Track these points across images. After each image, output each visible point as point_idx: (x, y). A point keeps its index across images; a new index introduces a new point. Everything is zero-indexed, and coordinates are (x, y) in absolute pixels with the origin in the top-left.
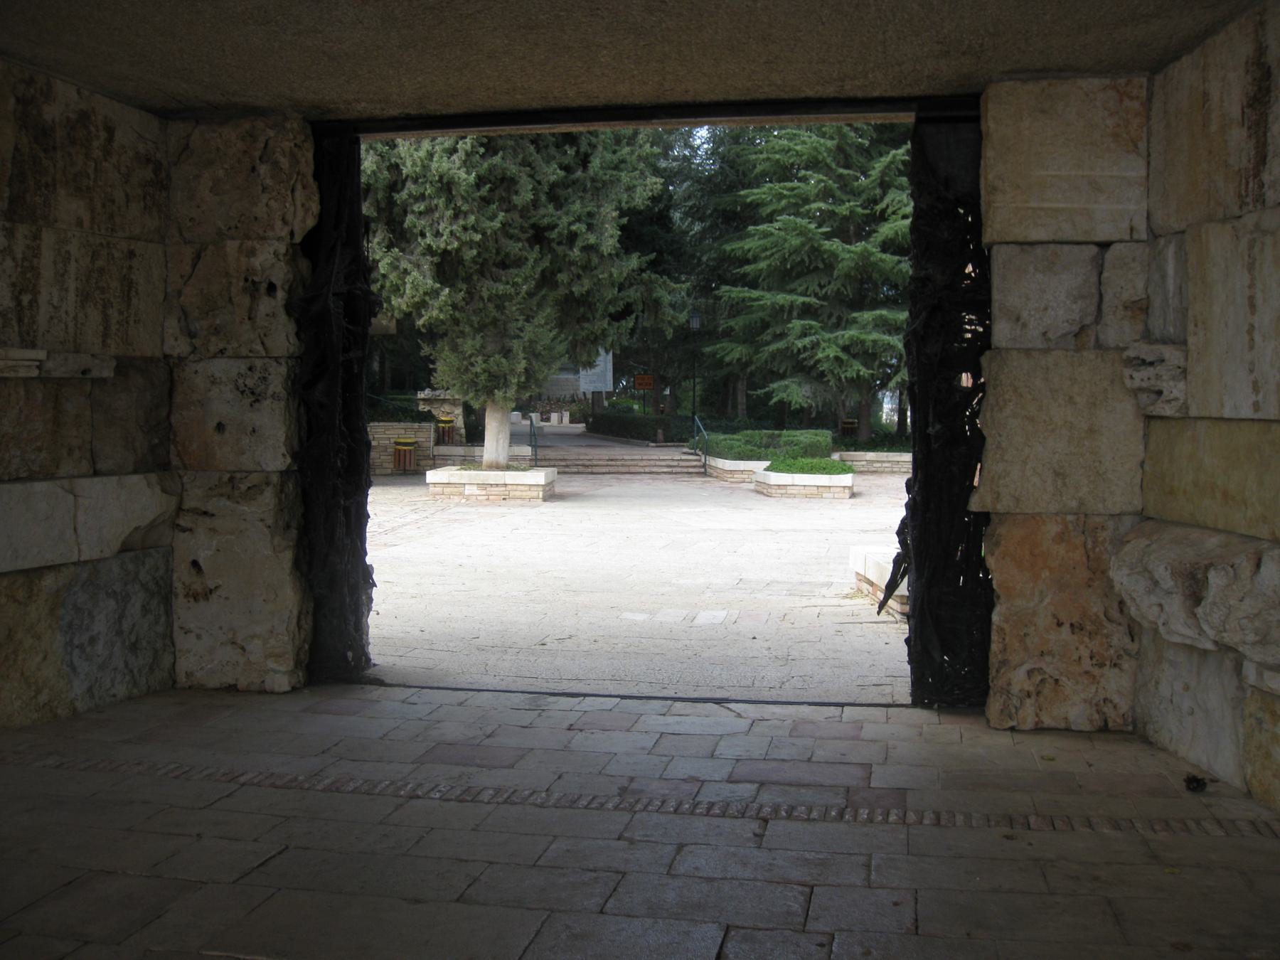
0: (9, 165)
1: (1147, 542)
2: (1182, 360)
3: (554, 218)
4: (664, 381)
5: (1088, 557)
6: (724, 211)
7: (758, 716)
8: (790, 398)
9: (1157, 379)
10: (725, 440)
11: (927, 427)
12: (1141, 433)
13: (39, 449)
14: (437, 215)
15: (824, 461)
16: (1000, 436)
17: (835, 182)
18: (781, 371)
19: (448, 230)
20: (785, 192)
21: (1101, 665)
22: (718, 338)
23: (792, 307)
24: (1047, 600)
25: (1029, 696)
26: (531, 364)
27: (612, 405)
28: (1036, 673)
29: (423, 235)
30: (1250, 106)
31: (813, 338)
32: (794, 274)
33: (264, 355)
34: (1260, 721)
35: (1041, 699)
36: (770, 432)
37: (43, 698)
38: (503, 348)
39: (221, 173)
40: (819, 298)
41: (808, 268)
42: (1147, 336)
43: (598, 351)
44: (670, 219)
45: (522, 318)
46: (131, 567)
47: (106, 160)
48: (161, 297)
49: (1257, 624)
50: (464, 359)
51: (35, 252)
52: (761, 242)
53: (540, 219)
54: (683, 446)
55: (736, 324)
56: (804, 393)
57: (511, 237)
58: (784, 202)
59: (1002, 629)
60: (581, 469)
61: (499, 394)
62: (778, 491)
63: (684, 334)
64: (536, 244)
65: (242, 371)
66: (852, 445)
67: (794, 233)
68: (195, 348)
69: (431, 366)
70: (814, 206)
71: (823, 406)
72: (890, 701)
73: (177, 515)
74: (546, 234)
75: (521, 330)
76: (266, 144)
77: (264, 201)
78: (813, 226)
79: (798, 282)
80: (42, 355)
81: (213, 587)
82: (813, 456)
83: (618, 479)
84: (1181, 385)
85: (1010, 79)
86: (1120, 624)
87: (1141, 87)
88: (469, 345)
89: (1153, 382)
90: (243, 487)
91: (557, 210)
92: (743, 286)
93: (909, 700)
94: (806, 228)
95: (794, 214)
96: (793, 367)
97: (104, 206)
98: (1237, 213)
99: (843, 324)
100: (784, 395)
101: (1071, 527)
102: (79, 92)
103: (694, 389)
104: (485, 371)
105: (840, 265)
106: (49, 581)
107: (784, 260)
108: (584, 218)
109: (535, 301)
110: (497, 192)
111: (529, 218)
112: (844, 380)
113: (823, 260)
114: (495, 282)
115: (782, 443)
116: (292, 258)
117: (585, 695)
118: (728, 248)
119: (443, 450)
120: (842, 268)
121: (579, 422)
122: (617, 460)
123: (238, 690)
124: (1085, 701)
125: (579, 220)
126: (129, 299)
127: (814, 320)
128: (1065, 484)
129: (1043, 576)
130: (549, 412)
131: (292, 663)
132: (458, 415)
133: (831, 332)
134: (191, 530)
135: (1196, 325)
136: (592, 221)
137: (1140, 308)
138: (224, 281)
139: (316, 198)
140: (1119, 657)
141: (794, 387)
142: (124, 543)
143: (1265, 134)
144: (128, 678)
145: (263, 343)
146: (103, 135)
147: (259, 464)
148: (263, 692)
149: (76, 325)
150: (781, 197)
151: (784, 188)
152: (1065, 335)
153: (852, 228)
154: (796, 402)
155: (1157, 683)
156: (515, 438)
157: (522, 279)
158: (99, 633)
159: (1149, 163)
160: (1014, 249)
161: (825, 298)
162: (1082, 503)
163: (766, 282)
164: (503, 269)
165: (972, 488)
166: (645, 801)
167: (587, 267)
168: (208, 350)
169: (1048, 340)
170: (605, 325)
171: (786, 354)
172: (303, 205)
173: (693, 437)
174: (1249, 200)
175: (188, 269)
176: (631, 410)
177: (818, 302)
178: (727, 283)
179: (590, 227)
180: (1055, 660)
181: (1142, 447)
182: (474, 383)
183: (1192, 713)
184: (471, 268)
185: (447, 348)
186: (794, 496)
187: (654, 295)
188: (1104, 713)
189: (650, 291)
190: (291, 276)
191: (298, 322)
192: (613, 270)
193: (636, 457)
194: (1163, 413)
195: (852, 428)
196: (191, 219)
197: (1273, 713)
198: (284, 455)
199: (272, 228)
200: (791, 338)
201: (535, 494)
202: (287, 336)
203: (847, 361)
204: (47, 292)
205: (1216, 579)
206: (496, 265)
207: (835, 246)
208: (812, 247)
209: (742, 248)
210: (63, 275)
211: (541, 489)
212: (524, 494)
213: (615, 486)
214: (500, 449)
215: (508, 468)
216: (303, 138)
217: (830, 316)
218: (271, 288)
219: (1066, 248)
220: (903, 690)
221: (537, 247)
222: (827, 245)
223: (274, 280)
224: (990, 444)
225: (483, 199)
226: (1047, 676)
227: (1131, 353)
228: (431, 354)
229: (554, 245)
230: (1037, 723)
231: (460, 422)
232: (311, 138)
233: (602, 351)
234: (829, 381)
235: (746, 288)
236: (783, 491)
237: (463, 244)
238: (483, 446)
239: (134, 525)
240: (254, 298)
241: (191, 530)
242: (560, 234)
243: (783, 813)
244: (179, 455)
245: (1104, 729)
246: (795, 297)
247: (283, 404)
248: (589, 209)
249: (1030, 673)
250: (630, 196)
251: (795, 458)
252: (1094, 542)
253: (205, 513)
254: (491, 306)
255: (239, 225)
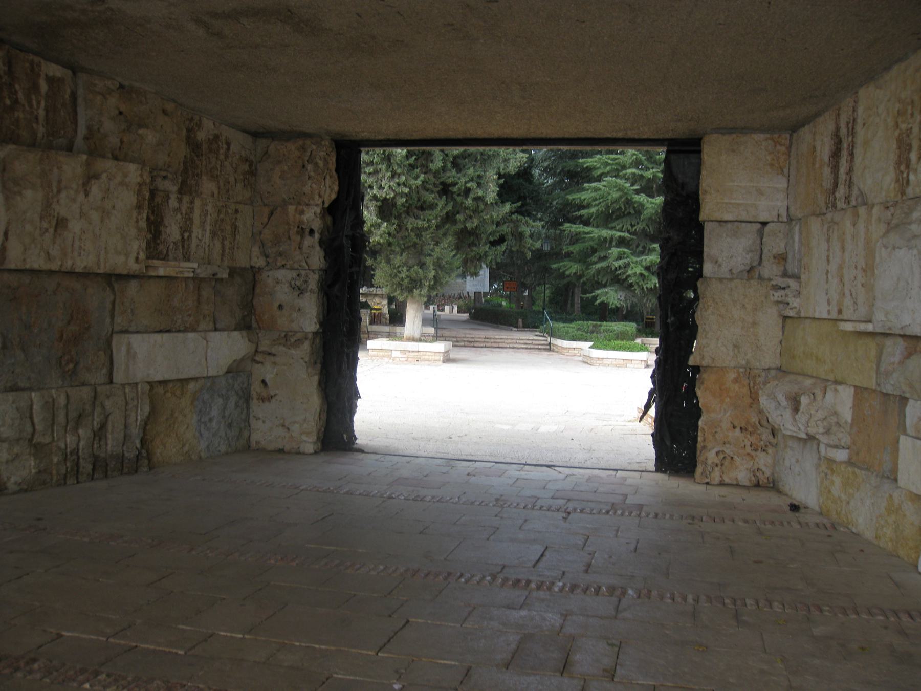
0: (182, 165)
1: (777, 383)
2: (798, 287)
3: (455, 179)
4: (524, 286)
5: (751, 391)
6: (569, 171)
7: (570, 473)
8: (608, 301)
9: (786, 296)
10: (564, 327)
11: (667, 319)
12: (781, 325)
13: (190, 315)
14: (381, 175)
15: (628, 343)
16: (705, 324)
17: (643, 155)
18: (603, 282)
19: (387, 186)
20: (609, 161)
21: (756, 450)
22: (562, 258)
23: (612, 238)
24: (728, 414)
25: (717, 466)
26: (437, 273)
27: (487, 302)
28: (721, 453)
29: (371, 187)
30: (833, 157)
31: (626, 260)
32: (614, 217)
33: (307, 268)
34: (826, 475)
35: (724, 468)
36: (595, 323)
37: (186, 448)
38: (420, 262)
39: (286, 168)
40: (630, 234)
41: (623, 213)
42: (785, 275)
43: (481, 266)
44: (532, 175)
45: (433, 243)
46: (230, 381)
47: (226, 160)
48: (250, 235)
49: (825, 424)
50: (395, 268)
51: (191, 210)
52: (593, 194)
53: (446, 179)
54: (536, 331)
55: (574, 249)
56: (619, 297)
57: (427, 190)
58: (608, 168)
59: (703, 429)
60: (467, 344)
61: (416, 292)
62: (598, 362)
63: (539, 255)
64: (444, 195)
65: (294, 277)
66: (650, 334)
67: (615, 190)
68: (268, 263)
69: (372, 273)
70: (629, 171)
71: (631, 306)
72: (644, 469)
73: (255, 355)
74: (450, 189)
75: (432, 250)
76: (311, 154)
77: (309, 184)
78: (628, 185)
79: (617, 222)
80: (195, 265)
81: (273, 395)
82: (622, 340)
83: (491, 351)
84: (798, 300)
85: (716, 133)
86: (767, 428)
87: (786, 139)
88: (397, 260)
89: (783, 298)
90: (292, 340)
91: (458, 173)
92: (580, 224)
93: (654, 469)
94: (623, 186)
95: (615, 176)
96: (612, 280)
97: (224, 185)
98: (825, 211)
99: (647, 251)
100: (605, 298)
101: (742, 375)
102: (214, 124)
103: (545, 292)
104: (407, 277)
105: (645, 212)
106: (192, 386)
107: (608, 207)
108: (475, 179)
109: (441, 232)
110: (419, 160)
111: (440, 178)
112: (645, 289)
113: (634, 208)
114: (416, 219)
115: (602, 331)
116: (323, 217)
117: (476, 461)
118: (570, 197)
119: (375, 328)
120: (646, 213)
121: (464, 313)
122: (491, 338)
123: (284, 452)
124: (747, 469)
125: (472, 180)
126: (235, 235)
127: (627, 248)
128: (739, 352)
129: (726, 401)
130: (444, 305)
131: (315, 438)
132: (385, 305)
133: (638, 257)
134: (262, 363)
135: (805, 269)
136: (480, 181)
137: (782, 258)
138: (286, 227)
139: (337, 183)
140: (766, 446)
141: (612, 293)
142: (228, 369)
143: (838, 172)
144: (226, 442)
145: (306, 262)
146: (225, 146)
147: (302, 328)
148: (299, 453)
149: (209, 250)
150: (607, 164)
151: (609, 158)
152: (742, 271)
153: (655, 186)
154: (613, 303)
155: (784, 459)
156: (425, 322)
157: (433, 217)
158: (214, 416)
159: (789, 180)
160: (716, 225)
161: (634, 233)
162: (748, 362)
163: (595, 221)
164: (422, 211)
165: (691, 352)
166: (509, 503)
167: (476, 211)
168: (276, 265)
169: (732, 274)
170: (487, 249)
171: (608, 270)
172: (330, 187)
173: (543, 325)
174: (830, 205)
175: (266, 220)
176: (500, 305)
177: (629, 236)
178: (569, 222)
179: (479, 185)
180: (731, 446)
181: (781, 333)
182: (400, 284)
183: (799, 475)
184: (401, 209)
185: (383, 261)
186: (608, 365)
187: (520, 230)
188: (758, 477)
189: (517, 227)
190: (322, 226)
191: (325, 251)
192: (493, 213)
193: (504, 337)
194: (789, 315)
195: (652, 323)
196: (268, 193)
197: (832, 470)
198: (315, 323)
199: (313, 199)
200: (610, 260)
201: (437, 358)
202: (319, 259)
203: (648, 277)
204: (196, 232)
205: (804, 400)
206: (417, 208)
207: (642, 199)
208: (627, 198)
209: (580, 198)
210: (204, 223)
211: (442, 355)
212: (431, 358)
213: (487, 354)
214: (415, 328)
215: (420, 340)
216: (331, 150)
217: (637, 247)
218: (312, 232)
219: (744, 224)
220: (651, 466)
221: (444, 197)
222: (637, 198)
223: (313, 228)
224: (700, 329)
225: (410, 165)
226: (726, 455)
227: (774, 283)
228: (372, 265)
229: (455, 196)
230: (721, 481)
231: (385, 310)
232: (335, 149)
233: (484, 266)
234: (635, 290)
235: (581, 226)
236: (601, 362)
237: (396, 194)
238: (404, 326)
239: (235, 358)
240: (302, 237)
241: (262, 363)
242: (459, 189)
243: (579, 511)
244: (257, 321)
245: (757, 485)
246: (614, 232)
247: (316, 295)
248: (479, 173)
249: (718, 453)
250: (506, 165)
251: (609, 341)
252: (754, 384)
253: (270, 354)
254: (413, 234)
255: (295, 197)
